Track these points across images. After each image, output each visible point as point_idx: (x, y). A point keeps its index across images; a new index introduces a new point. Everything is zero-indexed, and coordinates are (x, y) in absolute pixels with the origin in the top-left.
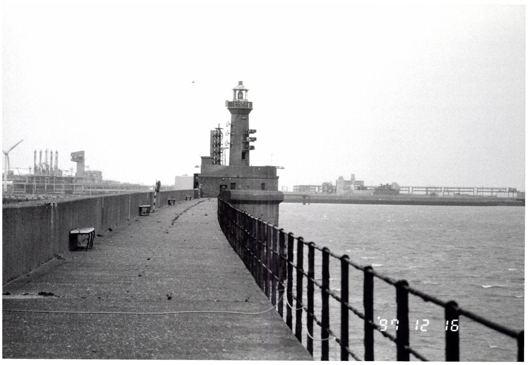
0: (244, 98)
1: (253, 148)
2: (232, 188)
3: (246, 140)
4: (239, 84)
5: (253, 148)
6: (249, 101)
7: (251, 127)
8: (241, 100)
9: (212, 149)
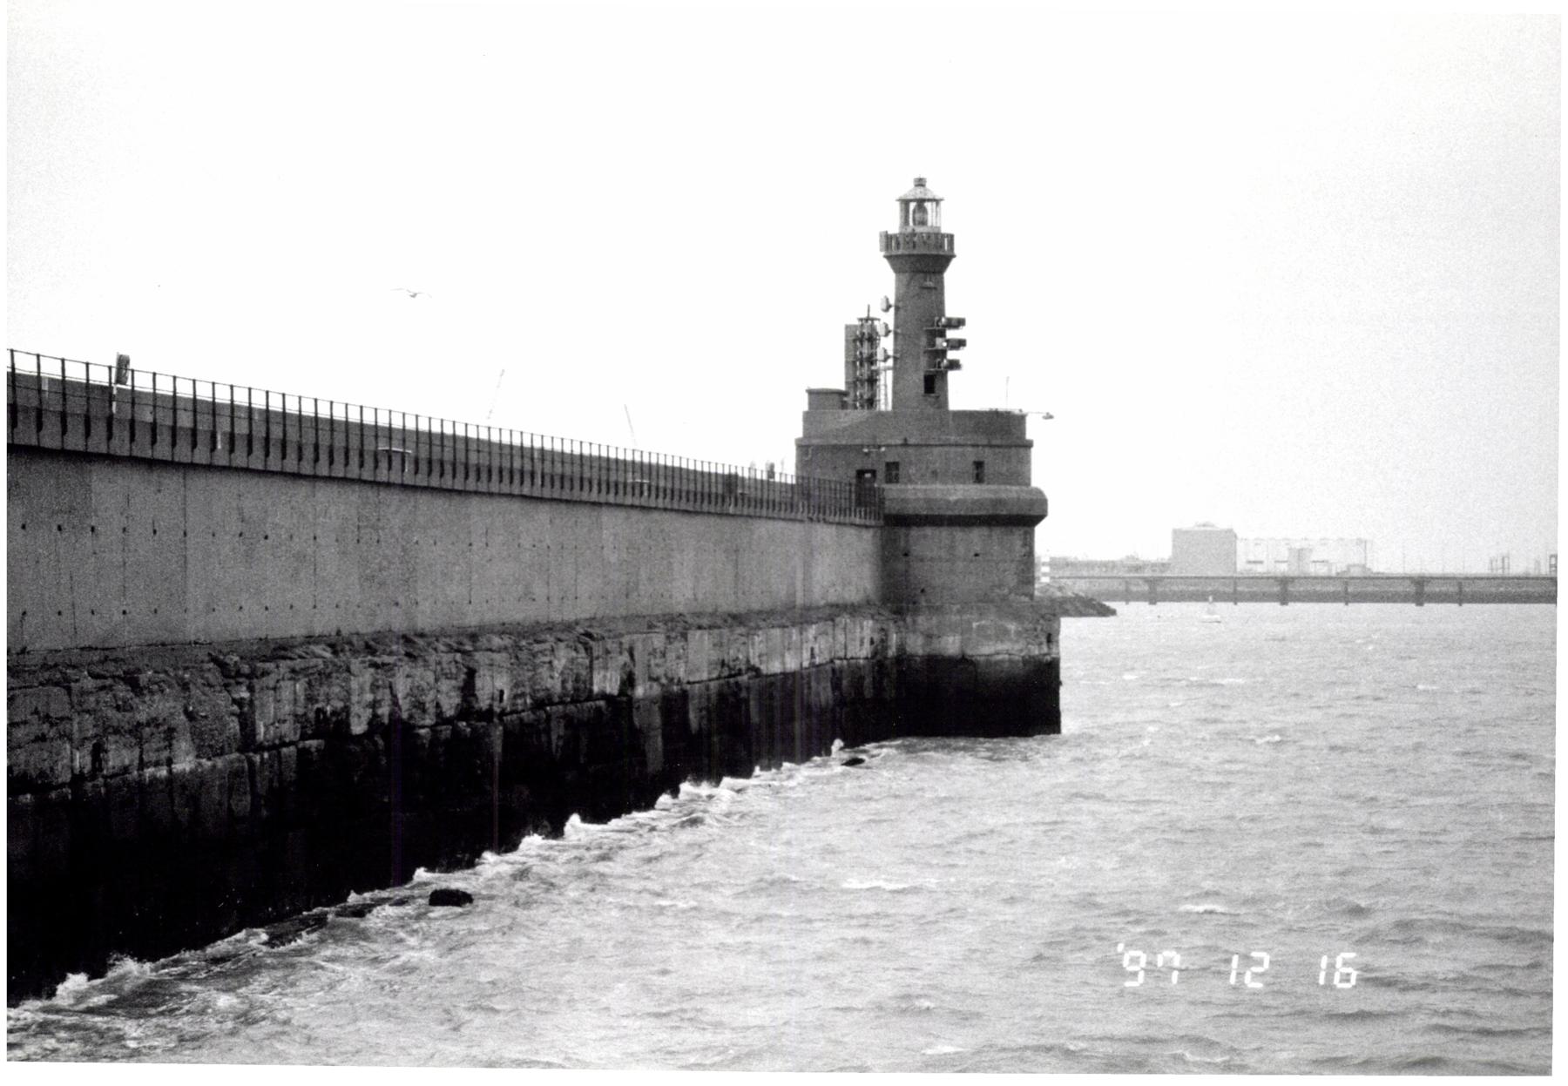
0: (929, 224)
2: (889, 481)
3: (934, 345)
4: (916, 186)
5: (955, 365)
6: (944, 230)
7: (951, 311)
8: (919, 229)
9: (851, 372)
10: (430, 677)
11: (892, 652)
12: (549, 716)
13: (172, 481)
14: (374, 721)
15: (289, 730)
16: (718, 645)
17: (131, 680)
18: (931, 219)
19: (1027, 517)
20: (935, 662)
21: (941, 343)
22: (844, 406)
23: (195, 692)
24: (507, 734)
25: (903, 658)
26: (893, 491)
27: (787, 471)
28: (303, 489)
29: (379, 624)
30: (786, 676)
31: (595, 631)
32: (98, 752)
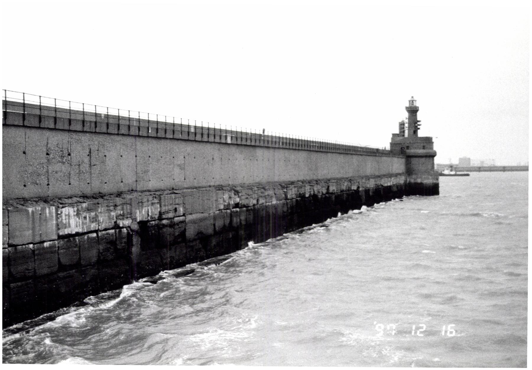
1: (419, 129)
5: (419, 129)
7: (418, 119)
10: (321, 187)
11: (408, 182)
12: (343, 194)
13: (271, 151)
14: (310, 195)
15: (294, 196)
16: (375, 181)
17: (264, 188)
18: (415, 104)
19: (432, 156)
20: (416, 184)
21: (416, 125)
22: (399, 136)
23: (276, 190)
24: (336, 197)
25: (410, 183)
26: (408, 151)
27: (388, 148)
28: (297, 152)
29: (311, 178)
30: (388, 186)
31: (352, 179)
32: (258, 200)
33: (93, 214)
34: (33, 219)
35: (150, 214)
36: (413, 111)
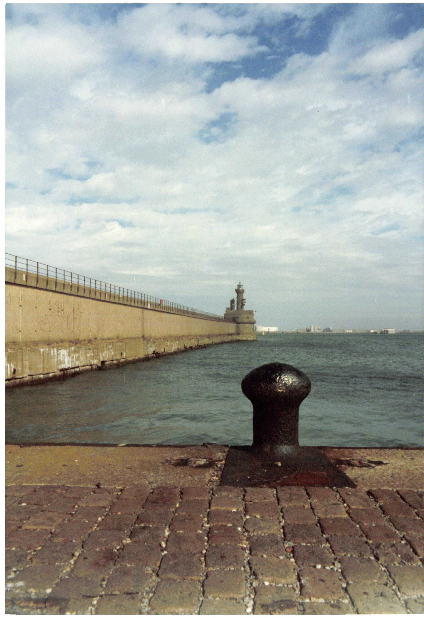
5: (244, 305)
7: (244, 298)
33: (77, 355)
34: (44, 357)
35: (107, 356)
36: (239, 292)
